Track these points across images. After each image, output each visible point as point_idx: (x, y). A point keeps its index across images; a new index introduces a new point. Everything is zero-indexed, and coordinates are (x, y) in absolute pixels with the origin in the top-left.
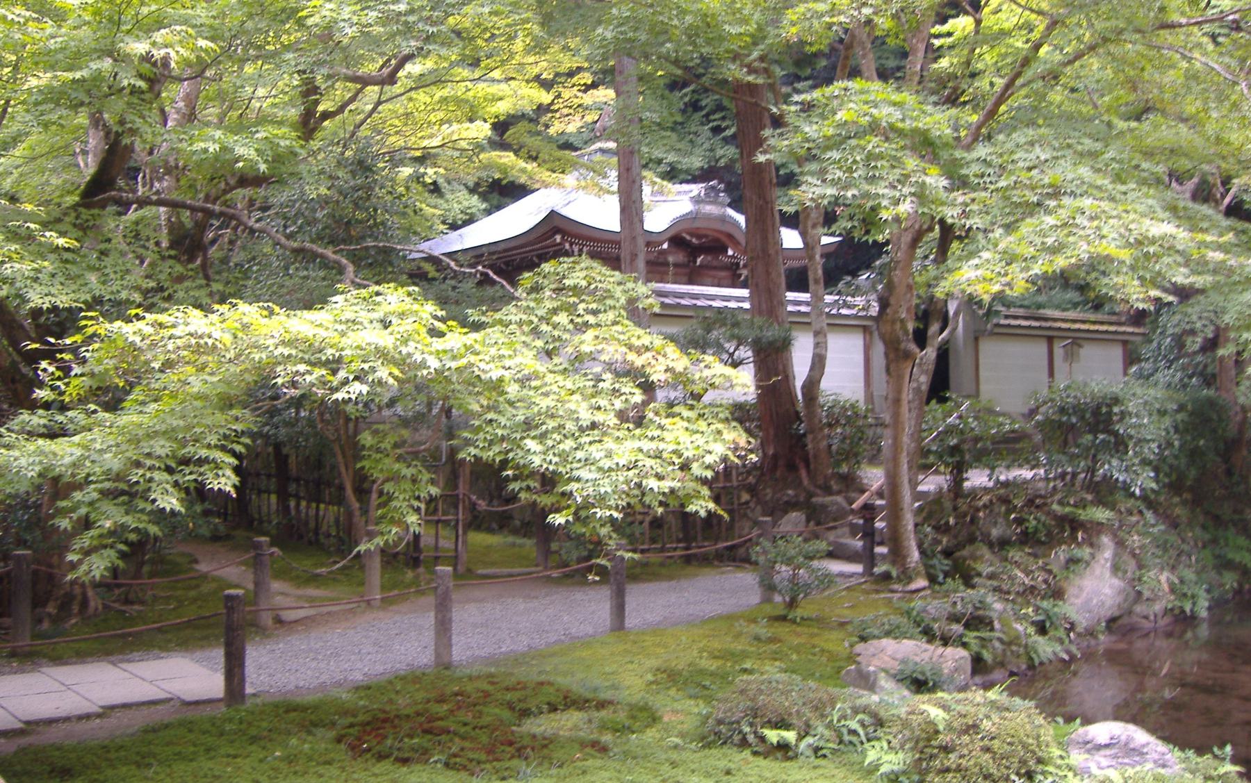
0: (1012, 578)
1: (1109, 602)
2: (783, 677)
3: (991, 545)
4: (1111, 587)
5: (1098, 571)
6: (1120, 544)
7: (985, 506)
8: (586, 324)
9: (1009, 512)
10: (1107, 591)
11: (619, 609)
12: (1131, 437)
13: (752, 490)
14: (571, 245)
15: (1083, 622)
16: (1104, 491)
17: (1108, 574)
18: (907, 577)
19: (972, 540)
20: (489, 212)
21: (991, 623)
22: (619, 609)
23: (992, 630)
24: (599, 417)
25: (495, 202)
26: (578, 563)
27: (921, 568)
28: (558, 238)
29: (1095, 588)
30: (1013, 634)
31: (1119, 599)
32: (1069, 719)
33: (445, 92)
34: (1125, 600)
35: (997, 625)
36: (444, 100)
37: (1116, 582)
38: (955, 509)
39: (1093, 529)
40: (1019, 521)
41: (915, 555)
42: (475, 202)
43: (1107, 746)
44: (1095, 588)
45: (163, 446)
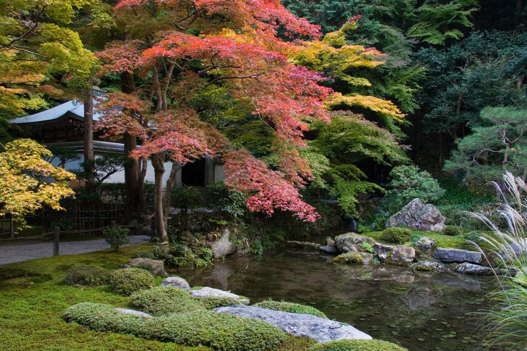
0: (195, 241)
1: (227, 249)
2: (102, 269)
3: (191, 231)
4: (228, 244)
5: (224, 239)
6: (232, 232)
7: (190, 219)
8: (26, 158)
9: (197, 221)
10: (226, 246)
11: (56, 249)
12: (235, 200)
13: (122, 212)
14: (76, 123)
15: (217, 255)
16: (228, 217)
17: (227, 240)
18: (162, 240)
19: (185, 230)
20: (50, 107)
21: (184, 255)
22: (56, 249)
23: (184, 256)
24: (22, 188)
25: (52, 103)
26: (5, 232)
27: (167, 238)
28: (71, 121)
29: (223, 245)
30: (190, 258)
31: (230, 248)
32: (163, 277)
33: (22, 63)
34: (232, 249)
35: (185, 255)
36: (23, 66)
37: (230, 243)
38: (182, 220)
39: (221, 228)
40: (200, 224)
41: (165, 234)
42: (44, 103)
43: (171, 283)
44: (223, 245)
45: (321, 163)
